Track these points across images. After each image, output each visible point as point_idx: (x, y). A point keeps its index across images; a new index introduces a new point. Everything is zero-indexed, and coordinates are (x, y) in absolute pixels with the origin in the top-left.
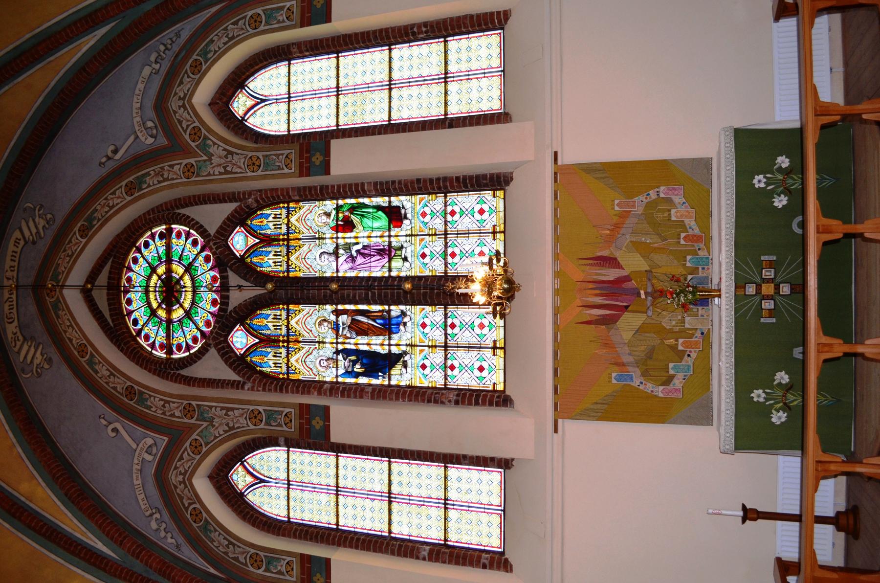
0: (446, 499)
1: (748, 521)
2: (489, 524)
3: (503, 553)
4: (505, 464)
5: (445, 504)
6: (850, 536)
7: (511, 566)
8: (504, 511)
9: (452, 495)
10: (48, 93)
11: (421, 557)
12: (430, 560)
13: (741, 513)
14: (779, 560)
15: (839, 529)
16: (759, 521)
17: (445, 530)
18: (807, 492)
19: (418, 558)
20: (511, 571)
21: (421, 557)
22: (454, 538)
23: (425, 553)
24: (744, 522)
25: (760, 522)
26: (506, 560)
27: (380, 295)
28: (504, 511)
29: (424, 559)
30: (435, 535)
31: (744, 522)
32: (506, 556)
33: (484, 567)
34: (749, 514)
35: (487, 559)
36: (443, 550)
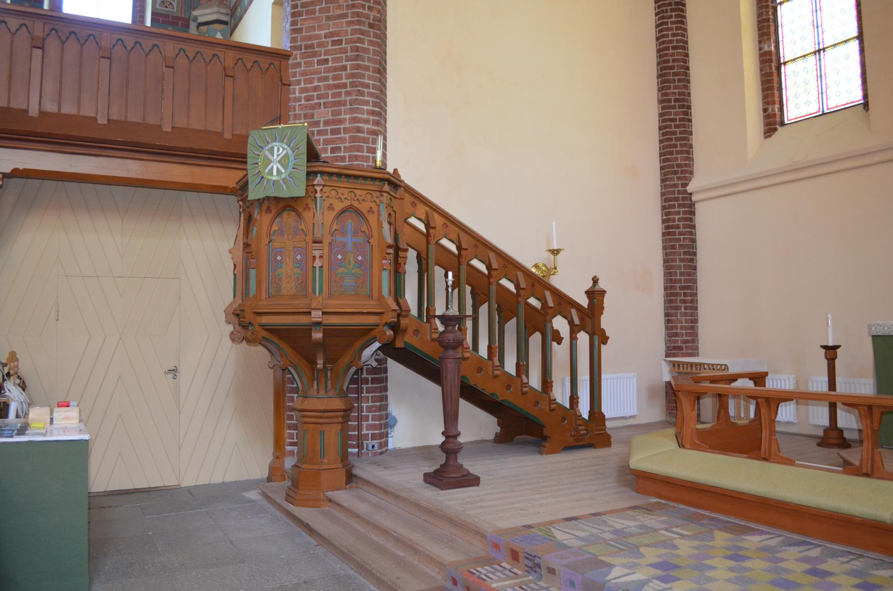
0: (824, 49)
1: (824, 351)
2: (807, 103)
3: (782, 124)
4: (866, 105)
5: (819, 51)
6: (820, 440)
7: (770, 136)
8: (824, 114)
9: (829, 54)
10: (5, 443)
11: (762, 46)
12: (761, 55)
13: (831, 344)
14: (766, 374)
15: (826, 431)
16: (826, 361)
17: (794, 60)
18: (852, 403)
19: (760, 42)
20: (766, 137)
21: (762, 46)
22: (788, 72)
23: (766, 48)
24: (823, 347)
25: (825, 362)
26: (775, 130)
27: (666, 55)
28: (824, 114)
29: (760, 49)
30: (788, 51)
31: (823, 347)
32: (779, 128)
33: (765, 110)
34: (831, 352)
35: (773, 110)
36: (774, 65)
